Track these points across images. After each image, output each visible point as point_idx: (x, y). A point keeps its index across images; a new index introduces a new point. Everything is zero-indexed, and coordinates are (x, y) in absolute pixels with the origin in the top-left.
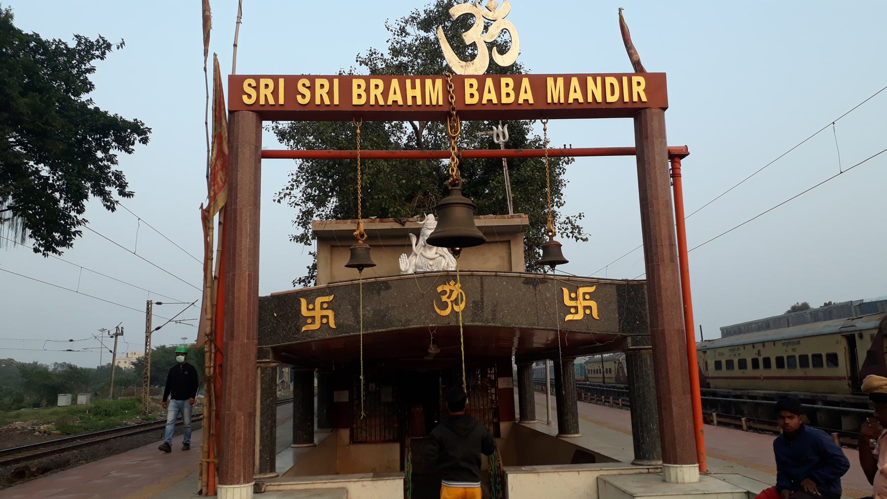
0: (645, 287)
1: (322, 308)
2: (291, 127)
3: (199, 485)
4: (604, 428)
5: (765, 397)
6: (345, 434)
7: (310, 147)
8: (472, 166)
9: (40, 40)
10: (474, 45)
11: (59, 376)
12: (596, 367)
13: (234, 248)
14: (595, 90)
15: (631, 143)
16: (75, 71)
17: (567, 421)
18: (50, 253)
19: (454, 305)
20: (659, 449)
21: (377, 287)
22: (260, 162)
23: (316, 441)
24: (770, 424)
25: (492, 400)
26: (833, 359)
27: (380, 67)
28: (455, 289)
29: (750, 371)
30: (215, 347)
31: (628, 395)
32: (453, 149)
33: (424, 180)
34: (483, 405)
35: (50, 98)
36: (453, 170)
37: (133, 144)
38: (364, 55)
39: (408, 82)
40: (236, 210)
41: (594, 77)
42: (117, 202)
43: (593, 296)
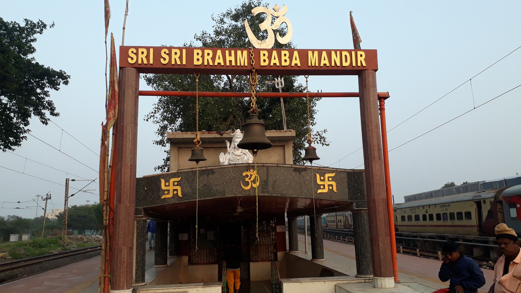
0: (364, 174)
1: (174, 185)
2: (154, 76)
3: (99, 290)
4: (339, 255)
5: (430, 237)
6: (186, 259)
7: (166, 88)
8: (262, 101)
9: (3, 21)
10: (266, 31)
11: (11, 223)
12: (333, 219)
13: (122, 149)
14: (336, 59)
15: (357, 90)
16: (24, 41)
17: (317, 251)
18: (7, 150)
19: (252, 183)
20: (371, 268)
21: (207, 172)
22: (138, 98)
23: (168, 264)
24: (432, 253)
25: (273, 239)
26: (468, 215)
27: (208, 42)
28: (253, 174)
29: (421, 222)
30: (110, 207)
31: (353, 236)
32: (253, 92)
33: (234, 108)
34: (268, 242)
35: (9, 57)
36: (253, 104)
37: (59, 85)
38: (199, 35)
39: (227, 52)
40: (123, 126)
41: (336, 51)
42: (49, 119)
43: (334, 179)
